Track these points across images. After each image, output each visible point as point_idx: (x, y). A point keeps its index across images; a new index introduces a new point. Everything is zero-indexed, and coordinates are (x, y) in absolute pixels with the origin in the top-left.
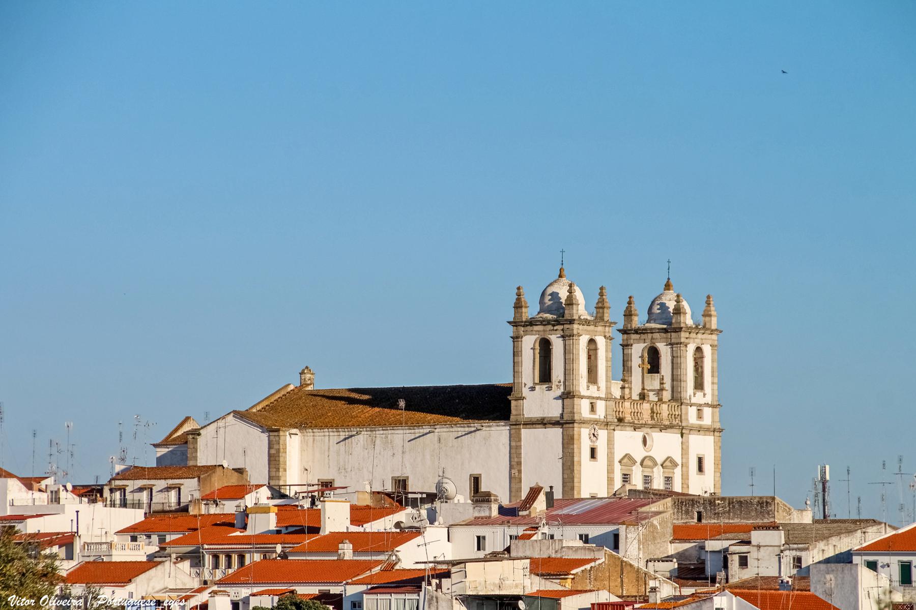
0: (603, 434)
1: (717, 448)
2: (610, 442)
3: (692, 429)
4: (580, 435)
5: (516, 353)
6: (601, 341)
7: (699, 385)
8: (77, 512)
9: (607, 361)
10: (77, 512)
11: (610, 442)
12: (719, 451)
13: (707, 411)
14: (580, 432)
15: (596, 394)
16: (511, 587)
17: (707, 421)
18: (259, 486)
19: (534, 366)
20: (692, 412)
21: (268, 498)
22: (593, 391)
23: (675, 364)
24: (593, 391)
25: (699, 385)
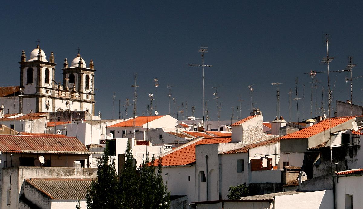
0: (51, 100)
1: (93, 108)
2: (53, 103)
3: (84, 101)
4: (41, 101)
5: (22, 73)
6: (50, 70)
7: (87, 86)
8: (8, 110)
9: (53, 76)
10: (8, 110)
11: (53, 103)
12: (94, 109)
13: (89, 96)
14: (41, 100)
15: (48, 87)
16: (65, 168)
17: (89, 99)
18: (76, 64)
19: (22, 77)
20: (85, 96)
21: (169, 192)
22: (47, 86)
23: (79, 80)
24: (47, 86)
25: (87, 86)
